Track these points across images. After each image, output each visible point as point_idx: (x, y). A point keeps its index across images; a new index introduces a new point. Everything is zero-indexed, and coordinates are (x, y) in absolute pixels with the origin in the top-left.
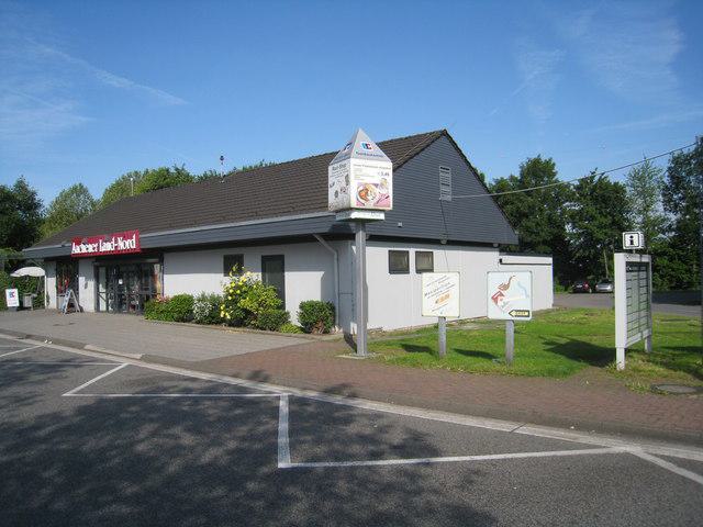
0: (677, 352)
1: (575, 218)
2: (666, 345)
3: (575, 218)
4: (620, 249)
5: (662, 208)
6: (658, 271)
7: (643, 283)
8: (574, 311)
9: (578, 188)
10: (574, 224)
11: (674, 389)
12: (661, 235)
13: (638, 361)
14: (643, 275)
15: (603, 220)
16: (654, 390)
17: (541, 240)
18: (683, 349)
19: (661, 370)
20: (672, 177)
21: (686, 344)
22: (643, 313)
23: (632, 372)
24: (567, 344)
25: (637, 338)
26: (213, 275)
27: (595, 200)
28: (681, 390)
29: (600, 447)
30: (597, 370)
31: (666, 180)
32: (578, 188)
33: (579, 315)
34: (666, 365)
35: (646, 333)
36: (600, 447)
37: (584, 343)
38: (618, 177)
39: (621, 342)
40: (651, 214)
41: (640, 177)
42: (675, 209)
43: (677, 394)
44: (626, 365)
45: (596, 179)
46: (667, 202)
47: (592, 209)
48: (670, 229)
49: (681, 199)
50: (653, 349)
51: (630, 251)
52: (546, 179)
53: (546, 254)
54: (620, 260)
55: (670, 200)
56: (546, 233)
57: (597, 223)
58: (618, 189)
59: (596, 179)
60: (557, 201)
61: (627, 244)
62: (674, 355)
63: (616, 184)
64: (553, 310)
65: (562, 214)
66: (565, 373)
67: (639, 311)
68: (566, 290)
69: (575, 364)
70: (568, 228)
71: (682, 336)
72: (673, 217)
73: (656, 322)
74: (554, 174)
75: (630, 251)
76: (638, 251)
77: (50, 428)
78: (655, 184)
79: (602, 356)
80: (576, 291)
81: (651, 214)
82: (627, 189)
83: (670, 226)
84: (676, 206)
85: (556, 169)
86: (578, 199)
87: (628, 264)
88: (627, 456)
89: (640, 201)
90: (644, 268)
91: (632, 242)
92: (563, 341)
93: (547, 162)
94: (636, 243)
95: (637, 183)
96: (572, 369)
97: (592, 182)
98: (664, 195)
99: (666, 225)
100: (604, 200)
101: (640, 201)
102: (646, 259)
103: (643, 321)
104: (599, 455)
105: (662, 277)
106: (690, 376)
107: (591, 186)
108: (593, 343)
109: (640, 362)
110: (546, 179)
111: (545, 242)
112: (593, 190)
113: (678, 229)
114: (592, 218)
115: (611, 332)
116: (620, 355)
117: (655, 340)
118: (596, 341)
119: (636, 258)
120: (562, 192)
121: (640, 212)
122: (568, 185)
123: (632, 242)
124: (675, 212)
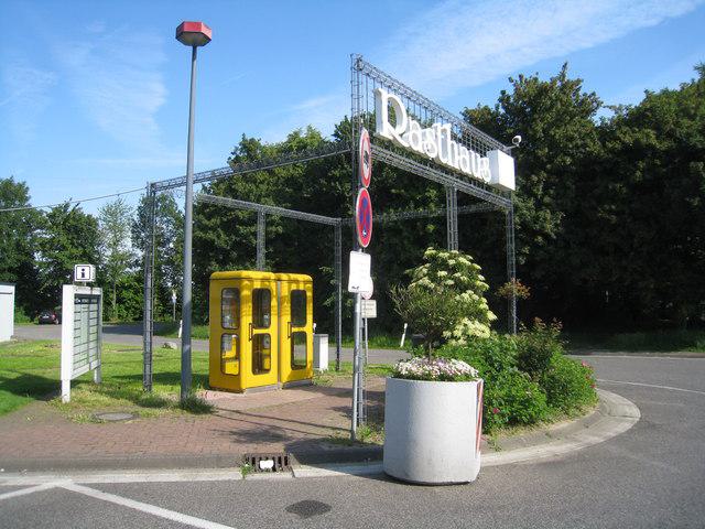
0: (124, 381)
1: (45, 246)
2: (118, 374)
3: (45, 246)
4: (70, 282)
5: (130, 244)
6: (124, 303)
7: (94, 315)
8: (35, 342)
9: (51, 216)
10: (44, 251)
11: (111, 417)
12: (127, 270)
13: (86, 393)
14: (94, 307)
15: (74, 251)
16: (95, 420)
17: (7, 267)
18: (129, 377)
19: (105, 399)
20: (141, 216)
21: (127, 373)
22: (92, 345)
23: (78, 403)
24: (18, 378)
25: (84, 369)
26: (624, 358)
27: (68, 230)
28: (118, 417)
29: (21, 488)
30: (42, 404)
31: (136, 218)
32: (50, 216)
33: (37, 348)
34: (108, 393)
35: (94, 364)
36: (21, 488)
37: (36, 377)
38: (92, 209)
39: (66, 376)
40: (120, 248)
41: (113, 212)
42: (142, 246)
43: (114, 421)
44: (72, 398)
45: (70, 209)
46: (135, 238)
47: (63, 239)
48: (137, 263)
49: (148, 237)
50: (103, 379)
51: (80, 284)
52: (17, 202)
53: (10, 282)
54: (69, 292)
55: (138, 237)
56: (12, 260)
57: (67, 253)
58: (91, 222)
59: (70, 209)
60: (28, 227)
61: (78, 276)
62: (120, 384)
63: (89, 216)
64: (11, 343)
65: (32, 241)
66: (6, 411)
67: (88, 342)
68: (32, 320)
69: (20, 399)
70: (38, 256)
71: (134, 365)
72: (140, 253)
73: (105, 350)
74: (27, 199)
75: (80, 284)
76: (89, 284)
77: (596, 438)
78: (124, 220)
79: (44, 389)
80: (42, 322)
81: (120, 248)
82: (100, 222)
83: (137, 261)
84: (143, 243)
85: (29, 194)
86: (50, 228)
87: (76, 296)
88: (56, 490)
89: (111, 235)
90: (95, 301)
91: (83, 275)
92: (13, 376)
93: (21, 186)
94: (87, 276)
95: (109, 218)
96: (14, 406)
97: (65, 211)
98: (133, 232)
99: (133, 259)
100: (76, 232)
101: (111, 235)
102: (97, 291)
103: (92, 352)
104: (27, 496)
105: (127, 309)
106: (130, 403)
107: (64, 216)
108: (45, 376)
109: (88, 393)
110: (17, 202)
111: (10, 270)
112: (66, 221)
113: (143, 265)
114: (63, 248)
115: (56, 364)
116: (66, 387)
117: (106, 370)
118: (49, 374)
119: (86, 291)
120: (33, 219)
121: (110, 245)
122: (41, 212)
123: (83, 275)
124: (142, 249)
